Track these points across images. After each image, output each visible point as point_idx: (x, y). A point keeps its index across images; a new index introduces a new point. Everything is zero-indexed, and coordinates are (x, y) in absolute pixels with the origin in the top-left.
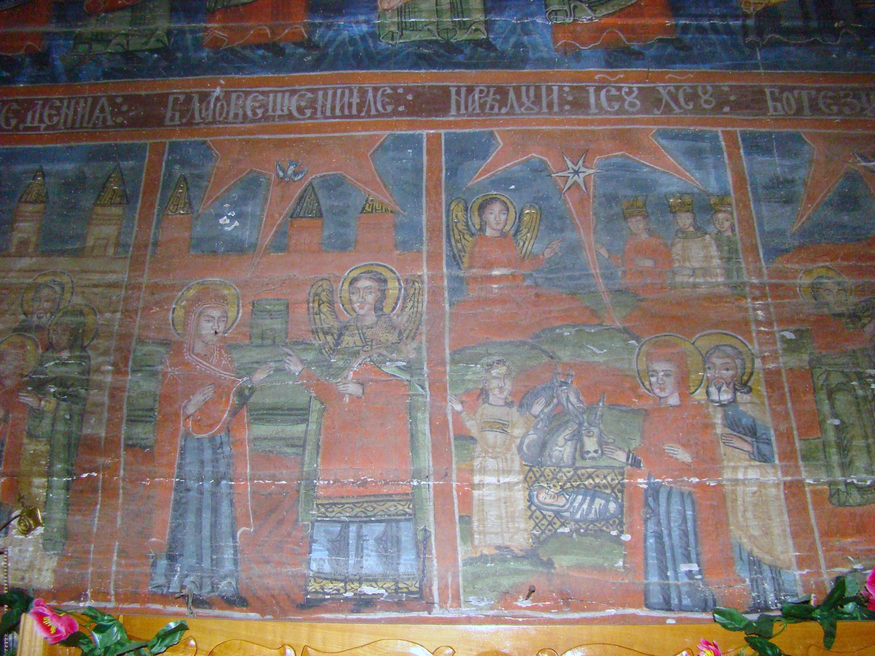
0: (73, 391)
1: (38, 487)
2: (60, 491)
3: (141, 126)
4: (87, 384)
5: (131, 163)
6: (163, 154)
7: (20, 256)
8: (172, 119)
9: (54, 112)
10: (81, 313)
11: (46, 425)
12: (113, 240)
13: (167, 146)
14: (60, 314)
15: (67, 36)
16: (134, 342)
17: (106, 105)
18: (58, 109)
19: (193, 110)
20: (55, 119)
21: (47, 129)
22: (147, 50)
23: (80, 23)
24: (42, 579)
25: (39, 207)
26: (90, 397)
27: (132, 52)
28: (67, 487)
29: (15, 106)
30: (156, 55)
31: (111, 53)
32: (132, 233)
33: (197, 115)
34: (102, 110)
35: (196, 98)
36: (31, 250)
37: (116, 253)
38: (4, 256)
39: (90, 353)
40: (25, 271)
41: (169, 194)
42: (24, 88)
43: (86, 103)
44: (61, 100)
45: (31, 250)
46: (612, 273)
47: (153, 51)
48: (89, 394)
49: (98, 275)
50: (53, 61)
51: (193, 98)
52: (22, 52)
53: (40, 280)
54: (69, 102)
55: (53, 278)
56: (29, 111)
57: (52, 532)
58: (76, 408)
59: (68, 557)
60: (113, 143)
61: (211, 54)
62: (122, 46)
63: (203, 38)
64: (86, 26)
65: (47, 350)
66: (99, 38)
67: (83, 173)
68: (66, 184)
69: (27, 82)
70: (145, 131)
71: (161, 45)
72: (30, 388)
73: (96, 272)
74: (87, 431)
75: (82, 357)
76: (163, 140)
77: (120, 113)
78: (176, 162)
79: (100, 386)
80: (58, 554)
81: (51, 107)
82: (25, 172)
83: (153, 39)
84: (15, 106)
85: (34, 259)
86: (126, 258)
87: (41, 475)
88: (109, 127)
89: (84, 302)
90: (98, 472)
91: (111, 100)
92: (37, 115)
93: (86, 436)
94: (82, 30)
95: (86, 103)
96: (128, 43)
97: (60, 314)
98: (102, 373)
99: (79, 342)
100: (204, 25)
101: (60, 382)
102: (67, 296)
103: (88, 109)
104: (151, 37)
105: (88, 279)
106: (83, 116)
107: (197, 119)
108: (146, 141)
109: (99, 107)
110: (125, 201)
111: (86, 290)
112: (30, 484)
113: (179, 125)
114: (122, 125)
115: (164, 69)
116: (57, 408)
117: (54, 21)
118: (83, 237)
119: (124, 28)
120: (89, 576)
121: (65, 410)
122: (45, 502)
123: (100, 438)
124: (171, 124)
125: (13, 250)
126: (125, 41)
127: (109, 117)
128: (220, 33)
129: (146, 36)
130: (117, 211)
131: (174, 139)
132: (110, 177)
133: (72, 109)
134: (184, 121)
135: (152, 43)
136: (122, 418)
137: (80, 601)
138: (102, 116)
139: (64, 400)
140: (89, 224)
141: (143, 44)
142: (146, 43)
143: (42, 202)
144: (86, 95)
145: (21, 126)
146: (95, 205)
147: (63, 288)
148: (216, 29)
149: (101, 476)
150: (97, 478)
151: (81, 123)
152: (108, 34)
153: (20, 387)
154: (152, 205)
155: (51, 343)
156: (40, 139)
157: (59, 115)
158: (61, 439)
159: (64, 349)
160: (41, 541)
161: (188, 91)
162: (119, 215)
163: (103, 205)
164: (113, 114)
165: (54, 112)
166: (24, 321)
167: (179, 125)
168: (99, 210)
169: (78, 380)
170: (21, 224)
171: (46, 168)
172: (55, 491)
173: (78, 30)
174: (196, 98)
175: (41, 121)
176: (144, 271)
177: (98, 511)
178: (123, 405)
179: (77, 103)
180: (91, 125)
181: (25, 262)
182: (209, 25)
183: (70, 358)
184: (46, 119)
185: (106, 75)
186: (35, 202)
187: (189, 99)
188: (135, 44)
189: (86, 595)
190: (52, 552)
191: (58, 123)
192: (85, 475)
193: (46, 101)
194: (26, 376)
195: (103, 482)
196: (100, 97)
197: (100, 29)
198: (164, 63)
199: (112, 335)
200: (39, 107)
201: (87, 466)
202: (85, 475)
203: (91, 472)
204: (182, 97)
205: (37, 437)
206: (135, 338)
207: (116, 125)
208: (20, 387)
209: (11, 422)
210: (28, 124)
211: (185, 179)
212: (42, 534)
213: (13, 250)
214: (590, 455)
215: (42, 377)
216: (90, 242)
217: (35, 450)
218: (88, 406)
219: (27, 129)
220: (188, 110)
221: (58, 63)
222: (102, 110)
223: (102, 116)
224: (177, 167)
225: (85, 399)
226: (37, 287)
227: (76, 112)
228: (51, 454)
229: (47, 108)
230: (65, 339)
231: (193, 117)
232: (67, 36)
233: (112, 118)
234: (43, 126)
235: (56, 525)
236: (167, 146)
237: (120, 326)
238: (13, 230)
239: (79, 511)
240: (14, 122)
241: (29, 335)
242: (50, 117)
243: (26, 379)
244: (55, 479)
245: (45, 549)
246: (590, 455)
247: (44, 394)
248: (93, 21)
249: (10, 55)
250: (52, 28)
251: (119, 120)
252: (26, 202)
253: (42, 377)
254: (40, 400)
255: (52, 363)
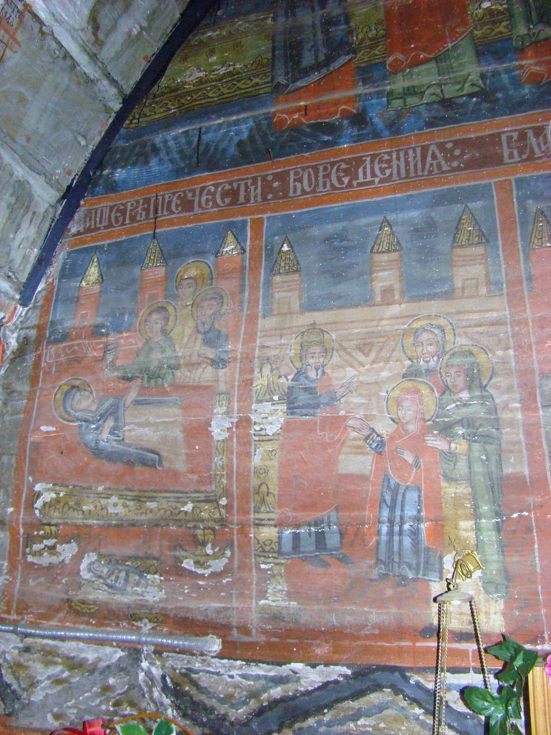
0: (484, 431)
1: (466, 530)
2: (490, 533)
3: (480, 167)
4: (497, 423)
5: (479, 204)
6: (511, 190)
7: (388, 304)
8: (511, 156)
9: (384, 166)
10: (471, 353)
11: (462, 466)
12: (482, 279)
13: (513, 183)
14: (448, 356)
15: (379, 95)
16: (537, 378)
17: (437, 152)
18: (389, 162)
19: (531, 144)
20: (388, 172)
21: (380, 182)
22: (463, 96)
23: (387, 82)
24: (491, 623)
25: (394, 256)
26: (504, 436)
27: (449, 100)
28: (498, 528)
29: (344, 166)
30: (475, 99)
31: (427, 104)
32: (500, 270)
33: (536, 149)
34: (434, 157)
35: (530, 134)
36: (397, 297)
37: (489, 291)
38: (370, 306)
39: (492, 391)
40: (397, 318)
41: (530, 229)
42: (347, 147)
43: (415, 152)
44: (389, 154)
45: (397, 297)
46: (542, 328)
47: (471, 95)
48: (502, 433)
49: (476, 314)
50: (371, 119)
51: (526, 134)
52: (338, 116)
53: (417, 325)
54: (398, 154)
55: (429, 322)
56: (359, 167)
57: (491, 574)
58: (491, 448)
59: (515, 600)
60: (454, 186)
61: (533, 90)
62: (437, 95)
63: (520, 76)
64: (394, 83)
65: (444, 393)
66: (411, 91)
67: (432, 218)
68: (416, 230)
69: (349, 142)
70: (485, 171)
71: (476, 89)
72: (436, 432)
73: (475, 312)
74: (508, 470)
75: (482, 397)
76: (508, 178)
77: (455, 158)
78: (527, 197)
79: (511, 423)
80: (503, 597)
81: (381, 161)
82: (369, 225)
83: (467, 85)
84: (344, 166)
85: (403, 306)
86: (502, 295)
87: (467, 518)
88: (445, 172)
89: (471, 343)
90: (529, 511)
91: (441, 146)
92: (368, 171)
93: (508, 477)
94: (393, 87)
95: (415, 152)
96: (442, 91)
97: (448, 356)
98: (511, 410)
99: (476, 382)
100: (517, 63)
101: (468, 423)
102: (449, 337)
103: (419, 158)
104: (465, 83)
105: (468, 320)
106: (416, 165)
107: (538, 154)
108: (490, 181)
109: (430, 154)
110: (484, 241)
111: (469, 330)
112: (456, 527)
113: (519, 162)
114: (458, 169)
115: (489, 110)
116: (470, 449)
117: (361, 84)
118: (450, 279)
119: (435, 79)
120: (544, 618)
121: (479, 451)
122: (477, 545)
123: (524, 477)
124: (511, 161)
125: (378, 299)
126: (439, 91)
127: (443, 163)
128: (538, 68)
129: (459, 83)
130: (480, 250)
131: (518, 176)
132: (461, 218)
133: (402, 160)
134: (524, 157)
135: (468, 89)
136: (544, 455)
137: (537, 644)
138: (435, 163)
139: (475, 441)
140: (452, 266)
141: (458, 90)
142: (462, 89)
143: (395, 251)
144: (413, 146)
145: (355, 183)
146: (453, 247)
147: (443, 331)
148: (531, 65)
149: (533, 515)
150: (529, 517)
151: (416, 172)
152: (422, 86)
153: (426, 430)
154: (514, 242)
155: (447, 386)
156: (377, 192)
157: (390, 167)
158: (481, 481)
159: (461, 391)
160: (480, 584)
161: (520, 127)
162: (482, 255)
163: (462, 247)
164: (446, 159)
165: (384, 166)
166: (411, 366)
167: (519, 162)
168: (458, 251)
169: (486, 419)
170: (380, 274)
171: (391, 217)
172: (485, 533)
173: (388, 88)
174: (530, 134)
175: (373, 175)
176: (525, 305)
177: (536, 550)
178: (541, 442)
179: (406, 154)
180: (426, 173)
181: (394, 310)
182: (524, 62)
183: (471, 399)
184: (378, 172)
185: (429, 125)
186: (388, 251)
187: (523, 135)
188: (450, 91)
189: (544, 638)
190: (496, 595)
191: (391, 174)
192: (515, 515)
193: (373, 157)
194: (429, 420)
195: (536, 520)
196: (429, 145)
197: (408, 83)
198: (485, 106)
199: (512, 373)
200: (368, 163)
201: (515, 506)
202: (515, 515)
203: (521, 511)
204: (515, 135)
205: (456, 480)
206: (537, 373)
207: (453, 170)
208: (426, 430)
209: (422, 466)
210: (361, 180)
211: (542, 212)
212: (480, 578)
213: (378, 299)
214: (494, 469)
215: (446, 420)
216: (459, 284)
217: (455, 493)
218: (503, 446)
219: (360, 185)
220: (525, 146)
221: (376, 120)
222: (434, 157)
223: (435, 163)
224: (530, 202)
225: (499, 439)
226: (416, 333)
227: (407, 163)
228: (474, 495)
229: (377, 161)
230: (460, 381)
231: (532, 151)
232: (379, 95)
233: (446, 163)
234: (377, 180)
235: (494, 568)
236: (513, 183)
237: (517, 362)
238: (372, 280)
239: (517, 551)
240: (346, 180)
241: (420, 380)
242: (382, 170)
243: (430, 423)
244: (483, 520)
245: (487, 592)
246: (494, 469)
247: (452, 437)
248: (399, 76)
249: (327, 120)
250: (361, 90)
251: (455, 164)
252: (378, 252)
253: (446, 420)
254: (450, 443)
255: (454, 405)
